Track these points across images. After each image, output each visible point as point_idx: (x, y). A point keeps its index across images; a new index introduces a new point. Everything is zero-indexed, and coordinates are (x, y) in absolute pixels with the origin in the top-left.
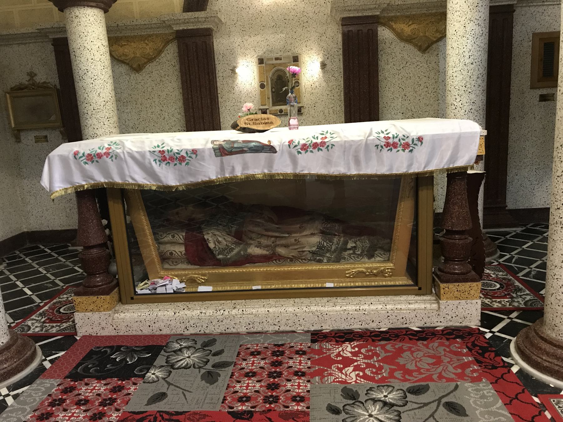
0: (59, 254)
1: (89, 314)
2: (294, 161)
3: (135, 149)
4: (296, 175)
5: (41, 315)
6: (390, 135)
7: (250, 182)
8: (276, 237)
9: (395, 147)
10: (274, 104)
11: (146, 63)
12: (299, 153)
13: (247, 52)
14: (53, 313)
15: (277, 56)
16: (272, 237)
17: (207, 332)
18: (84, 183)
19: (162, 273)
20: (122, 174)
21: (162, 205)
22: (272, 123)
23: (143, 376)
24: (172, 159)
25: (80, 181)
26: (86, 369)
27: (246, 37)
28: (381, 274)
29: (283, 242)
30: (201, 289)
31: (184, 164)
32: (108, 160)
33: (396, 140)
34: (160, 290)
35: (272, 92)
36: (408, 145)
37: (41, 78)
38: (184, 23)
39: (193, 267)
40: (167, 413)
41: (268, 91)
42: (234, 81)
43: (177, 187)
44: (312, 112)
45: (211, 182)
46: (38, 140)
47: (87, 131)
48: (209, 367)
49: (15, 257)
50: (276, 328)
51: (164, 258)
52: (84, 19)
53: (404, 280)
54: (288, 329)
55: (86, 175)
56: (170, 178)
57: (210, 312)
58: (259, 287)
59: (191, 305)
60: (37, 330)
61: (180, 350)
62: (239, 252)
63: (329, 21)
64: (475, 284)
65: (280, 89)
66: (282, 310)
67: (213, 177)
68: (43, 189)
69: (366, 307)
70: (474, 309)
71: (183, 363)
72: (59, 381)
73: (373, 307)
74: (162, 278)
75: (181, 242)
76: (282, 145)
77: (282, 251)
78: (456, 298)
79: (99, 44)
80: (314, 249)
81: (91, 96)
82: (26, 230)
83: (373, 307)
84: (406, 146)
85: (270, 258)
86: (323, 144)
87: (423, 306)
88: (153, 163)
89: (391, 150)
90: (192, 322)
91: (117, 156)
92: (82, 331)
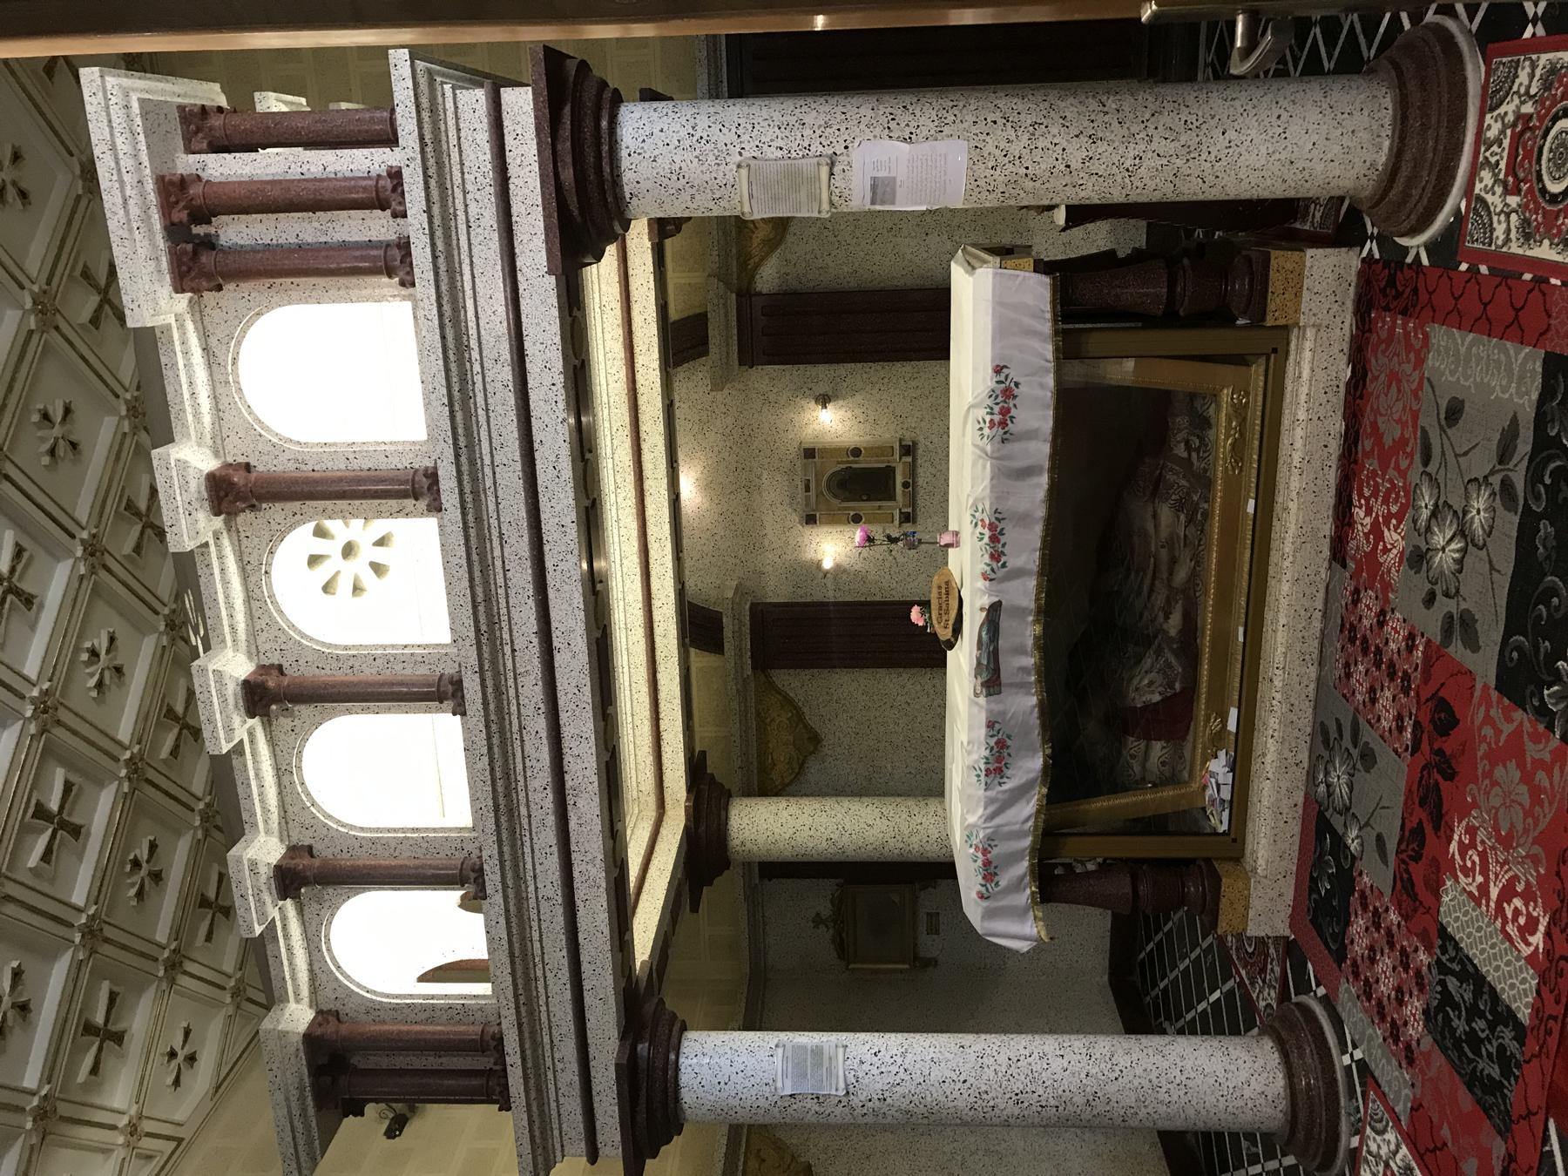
0: (1158, 929)
1: (1251, 913)
2: (1019, 573)
3: (980, 811)
4: (1041, 574)
5: (1252, 984)
6: (988, 418)
7: (1046, 646)
8: (1154, 578)
9: (1009, 410)
10: (892, 497)
11: (806, 726)
12: (1004, 566)
13: (792, 543)
14: (1252, 965)
15: (801, 487)
16: (1153, 584)
17: (1309, 730)
18: (1028, 891)
19: (1195, 786)
20: (1019, 835)
21: (1070, 778)
22: (947, 583)
23: (1354, 858)
24: (999, 759)
25: (1024, 897)
26: (1334, 936)
27: (766, 543)
28: (1240, 411)
29: (1164, 568)
30: (1232, 726)
31: (1009, 742)
32: (995, 851)
33: (997, 409)
34: (1226, 794)
35: (868, 500)
36: (1005, 396)
37: (826, 909)
38: (741, 656)
39: (1191, 732)
40: (1400, 843)
41: (865, 507)
42: (845, 571)
43: (1046, 757)
44: (912, 422)
45: (1041, 704)
46: (934, 930)
47: (933, 852)
48: (1355, 753)
49: (1157, 1006)
50: (1318, 615)
51: (1171, 779)
52: (747, 833)
53: (1257, 372)
54: (1321, 595)
55: (1016, 887)
56: (1031, 764)
57: (1273, 723)
58: (1241, 630)
59: (1257, 751)
60: (1273, 994)
61: (1328, 786)
62: (1173, 651)
63: (741, 386)
64: (1273, 262)
65: (867, 485)
66: (1284, 603)
67: (1034, 700)
68: (1034, 949)
69: (1297, 457)
70: (1324, 262)
71: (1345, 789)
72: (1343, 980)
73: (1299, 444)
74: (1205, 787)
75: (1143, 746)
76: (990, 592)
77: (1181, 575)
78: (1298, 295)
79: (785, 813)
80: (1182, 517)
81: (872, 840)
82: (1106, 978)
83: (1299, 444)
84: (1008, 394)
85: (1190, 597)
86: (992, 527)
87: (1307, 355)
88: (1005, 787)
89: (1012, 418)
90: (1287, 754)
91: (990, 838)
92: (1283, 929)
